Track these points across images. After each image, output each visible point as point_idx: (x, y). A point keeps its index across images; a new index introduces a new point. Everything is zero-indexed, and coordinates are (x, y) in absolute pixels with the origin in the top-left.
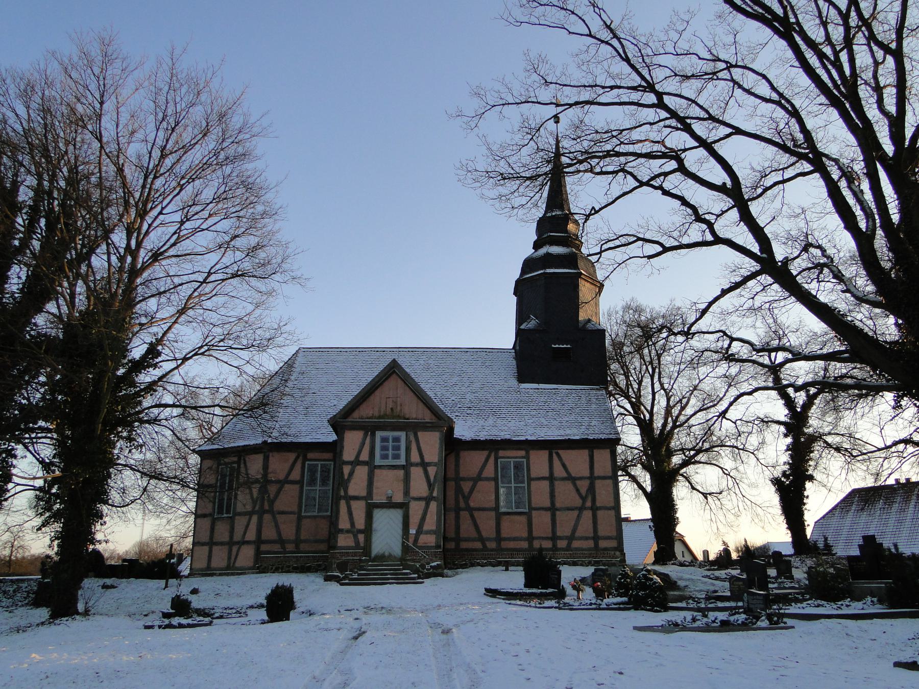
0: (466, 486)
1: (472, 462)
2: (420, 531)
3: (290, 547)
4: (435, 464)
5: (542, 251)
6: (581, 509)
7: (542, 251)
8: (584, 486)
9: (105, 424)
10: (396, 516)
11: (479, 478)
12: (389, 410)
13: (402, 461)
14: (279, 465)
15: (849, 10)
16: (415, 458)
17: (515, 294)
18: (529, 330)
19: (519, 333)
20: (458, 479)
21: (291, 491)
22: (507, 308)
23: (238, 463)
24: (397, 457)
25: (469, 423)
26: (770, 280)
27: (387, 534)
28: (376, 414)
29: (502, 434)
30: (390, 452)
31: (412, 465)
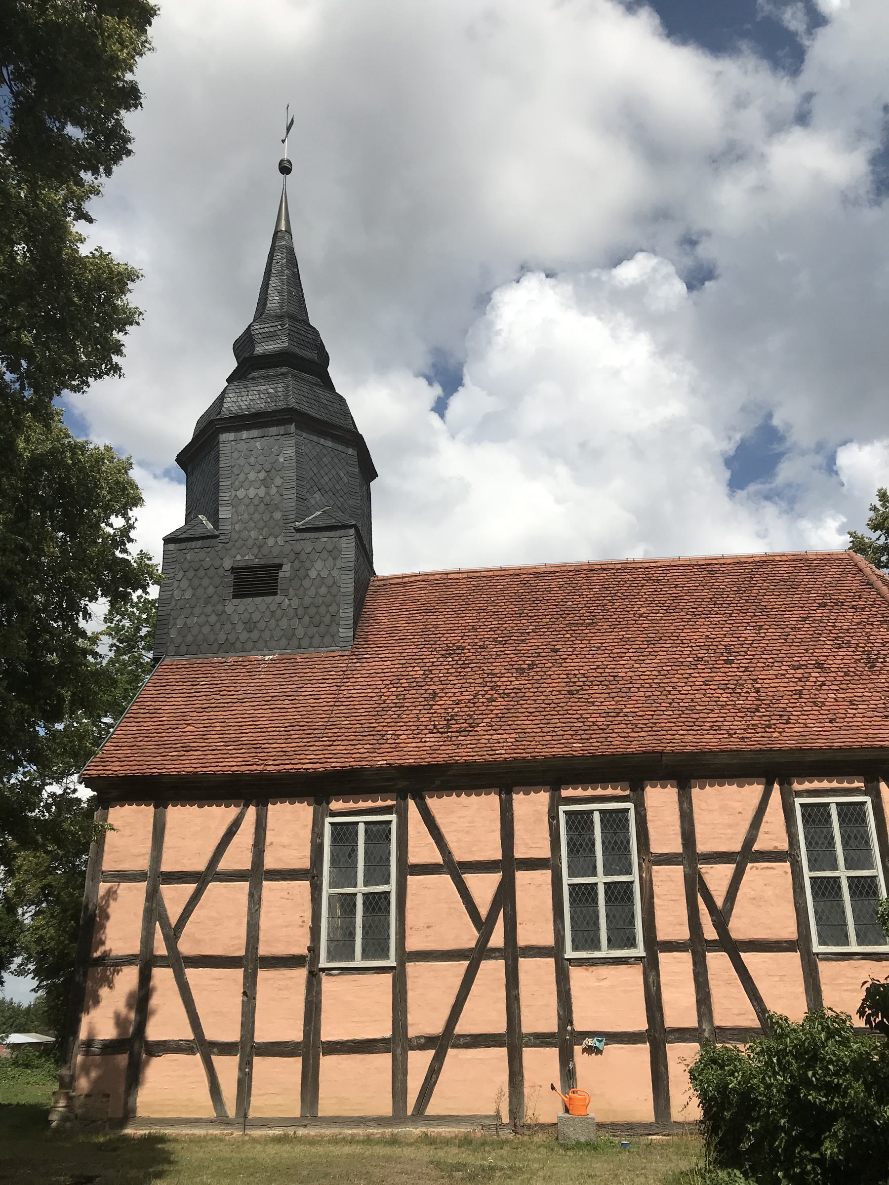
6: (475, 956)
8: (485, 888)
26: (355, 453)
29: (462, 752)
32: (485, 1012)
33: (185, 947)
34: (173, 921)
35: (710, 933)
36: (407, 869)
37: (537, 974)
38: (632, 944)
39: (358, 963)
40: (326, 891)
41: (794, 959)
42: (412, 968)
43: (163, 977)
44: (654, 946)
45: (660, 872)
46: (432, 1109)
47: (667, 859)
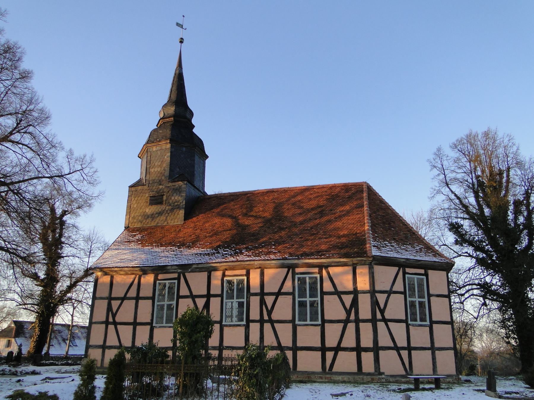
6: (346, 322)
8: (348, 300)
21: (285, 302)
32: (349, 341)
33: (118, 319)
34: (114, 312)
35: (266, 317)
36: (323, 293)
37: (366, 329)
38: (242, 320)
39: (164, 325)
40: (156, 303)
41: (404, 324)
42: (435, 326)
43: (381, 325)
44: (249, 321)
45: (252, 298)
46: (334, 370)
47: (255, 294)
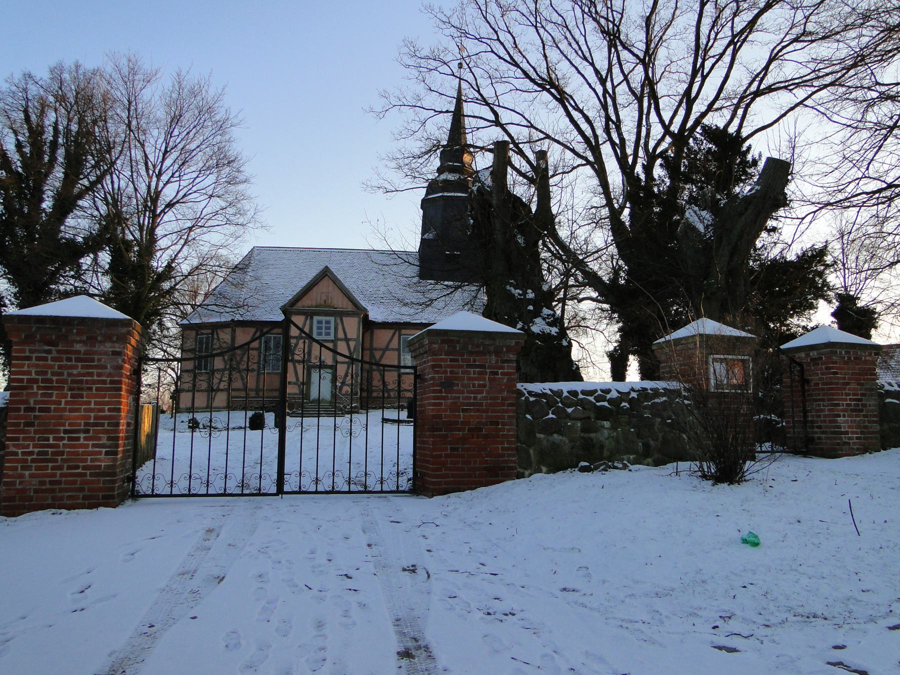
0: (378, 355)
1: (382, 337)
2: (343, 383)
3: (252, 394)
4: (354, 340)
5: (443, 177)
7: (443, 177)
9: (145, 316)
10: (327, 375)
11: (387, 348)
12: (323, 302)
13: (332, 337)
14: (243, 337)
15: (607, 77)
16: (341, 335)
17: (422, 208)
18: (429, 240)
19: (423, 241)
20: (372, 349)
22: (416, 217)
23: (212, 334)
24: (328, 334)
25: (382, 309)
27: (321, 387)
28: (314, 304)
30: (323, 331)
31: (339, 340)
